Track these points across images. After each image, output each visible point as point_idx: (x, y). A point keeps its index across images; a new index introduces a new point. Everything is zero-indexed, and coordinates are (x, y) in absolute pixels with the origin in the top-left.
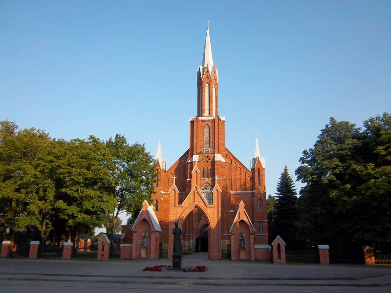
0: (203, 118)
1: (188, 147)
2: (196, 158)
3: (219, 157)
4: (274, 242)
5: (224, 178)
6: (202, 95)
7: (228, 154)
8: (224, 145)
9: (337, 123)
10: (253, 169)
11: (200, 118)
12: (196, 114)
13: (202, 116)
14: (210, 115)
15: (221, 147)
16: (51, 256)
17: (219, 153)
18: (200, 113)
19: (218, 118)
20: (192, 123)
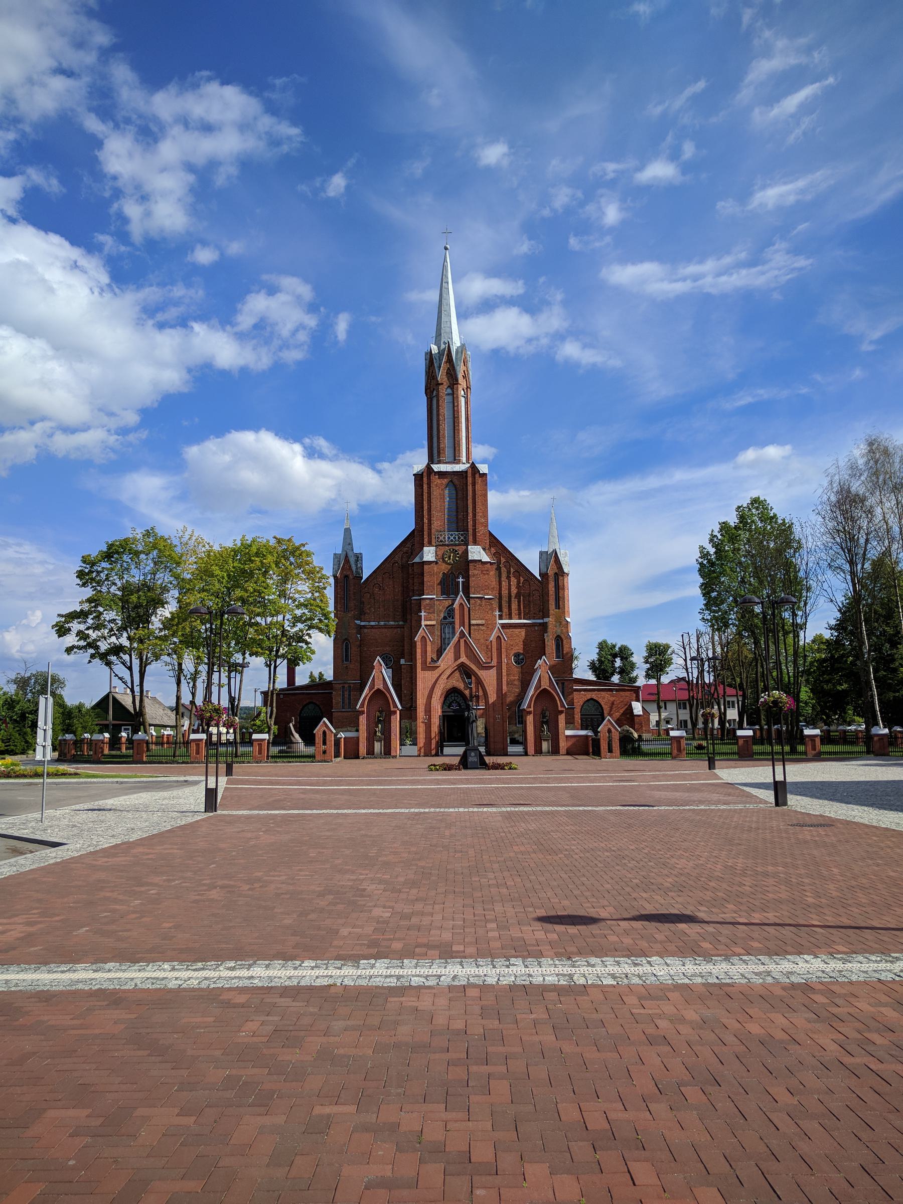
0: (443, 468)
1: (410, 526)
2: (429, 554)
3: (477, 553)
4: (318, 728)
5: (487, 594)
6: (438, 415)
7: (495, 545)
8: (486, 525)
9: (96, 153)
10: (544, 575)
11: (436, 467)
12: (425, 461)
13: (439, 462)
14: (456, 460)
15: (481, 530)
16: (852, 758)
17: (475, 543)
18: (435, 454)
19: (473, 466)
20: (418, 477)
